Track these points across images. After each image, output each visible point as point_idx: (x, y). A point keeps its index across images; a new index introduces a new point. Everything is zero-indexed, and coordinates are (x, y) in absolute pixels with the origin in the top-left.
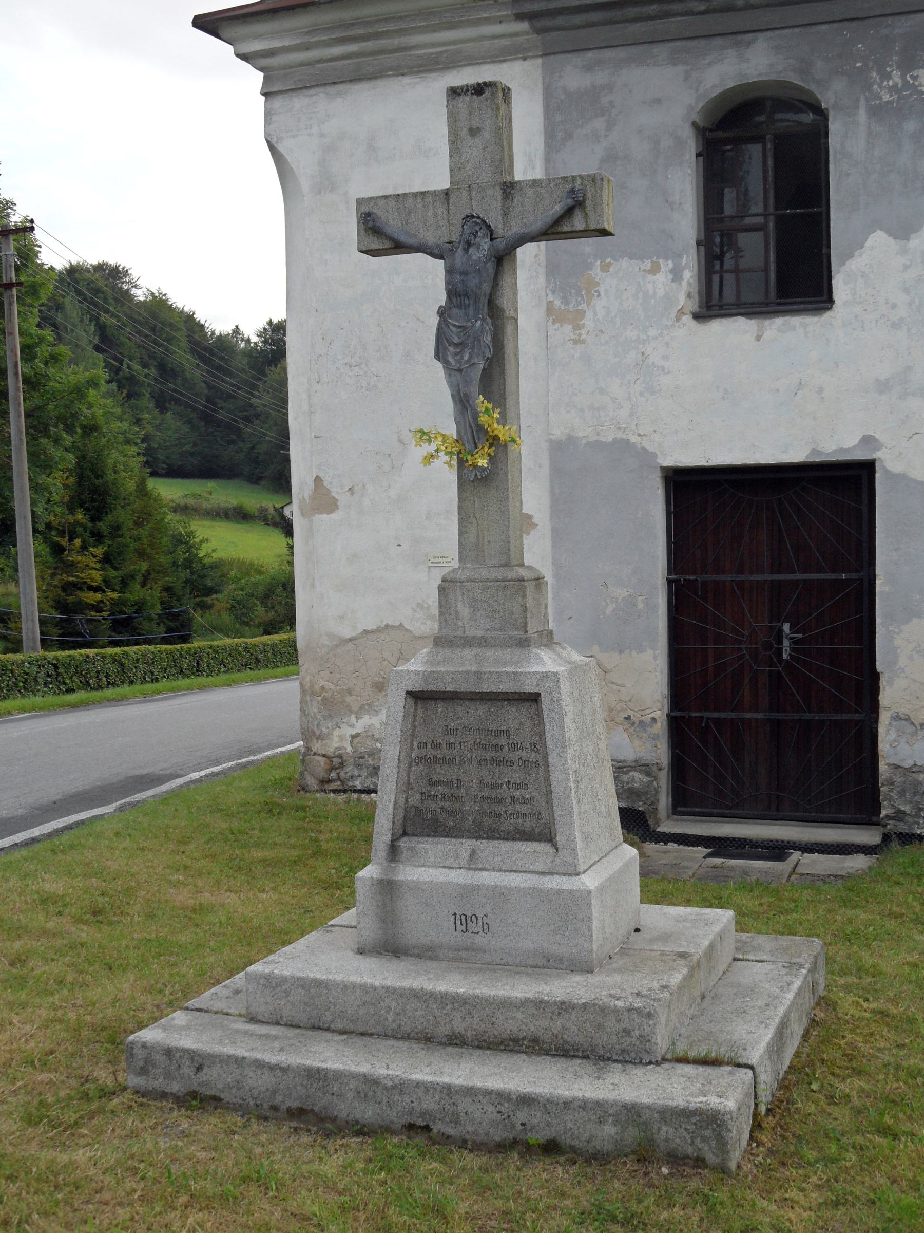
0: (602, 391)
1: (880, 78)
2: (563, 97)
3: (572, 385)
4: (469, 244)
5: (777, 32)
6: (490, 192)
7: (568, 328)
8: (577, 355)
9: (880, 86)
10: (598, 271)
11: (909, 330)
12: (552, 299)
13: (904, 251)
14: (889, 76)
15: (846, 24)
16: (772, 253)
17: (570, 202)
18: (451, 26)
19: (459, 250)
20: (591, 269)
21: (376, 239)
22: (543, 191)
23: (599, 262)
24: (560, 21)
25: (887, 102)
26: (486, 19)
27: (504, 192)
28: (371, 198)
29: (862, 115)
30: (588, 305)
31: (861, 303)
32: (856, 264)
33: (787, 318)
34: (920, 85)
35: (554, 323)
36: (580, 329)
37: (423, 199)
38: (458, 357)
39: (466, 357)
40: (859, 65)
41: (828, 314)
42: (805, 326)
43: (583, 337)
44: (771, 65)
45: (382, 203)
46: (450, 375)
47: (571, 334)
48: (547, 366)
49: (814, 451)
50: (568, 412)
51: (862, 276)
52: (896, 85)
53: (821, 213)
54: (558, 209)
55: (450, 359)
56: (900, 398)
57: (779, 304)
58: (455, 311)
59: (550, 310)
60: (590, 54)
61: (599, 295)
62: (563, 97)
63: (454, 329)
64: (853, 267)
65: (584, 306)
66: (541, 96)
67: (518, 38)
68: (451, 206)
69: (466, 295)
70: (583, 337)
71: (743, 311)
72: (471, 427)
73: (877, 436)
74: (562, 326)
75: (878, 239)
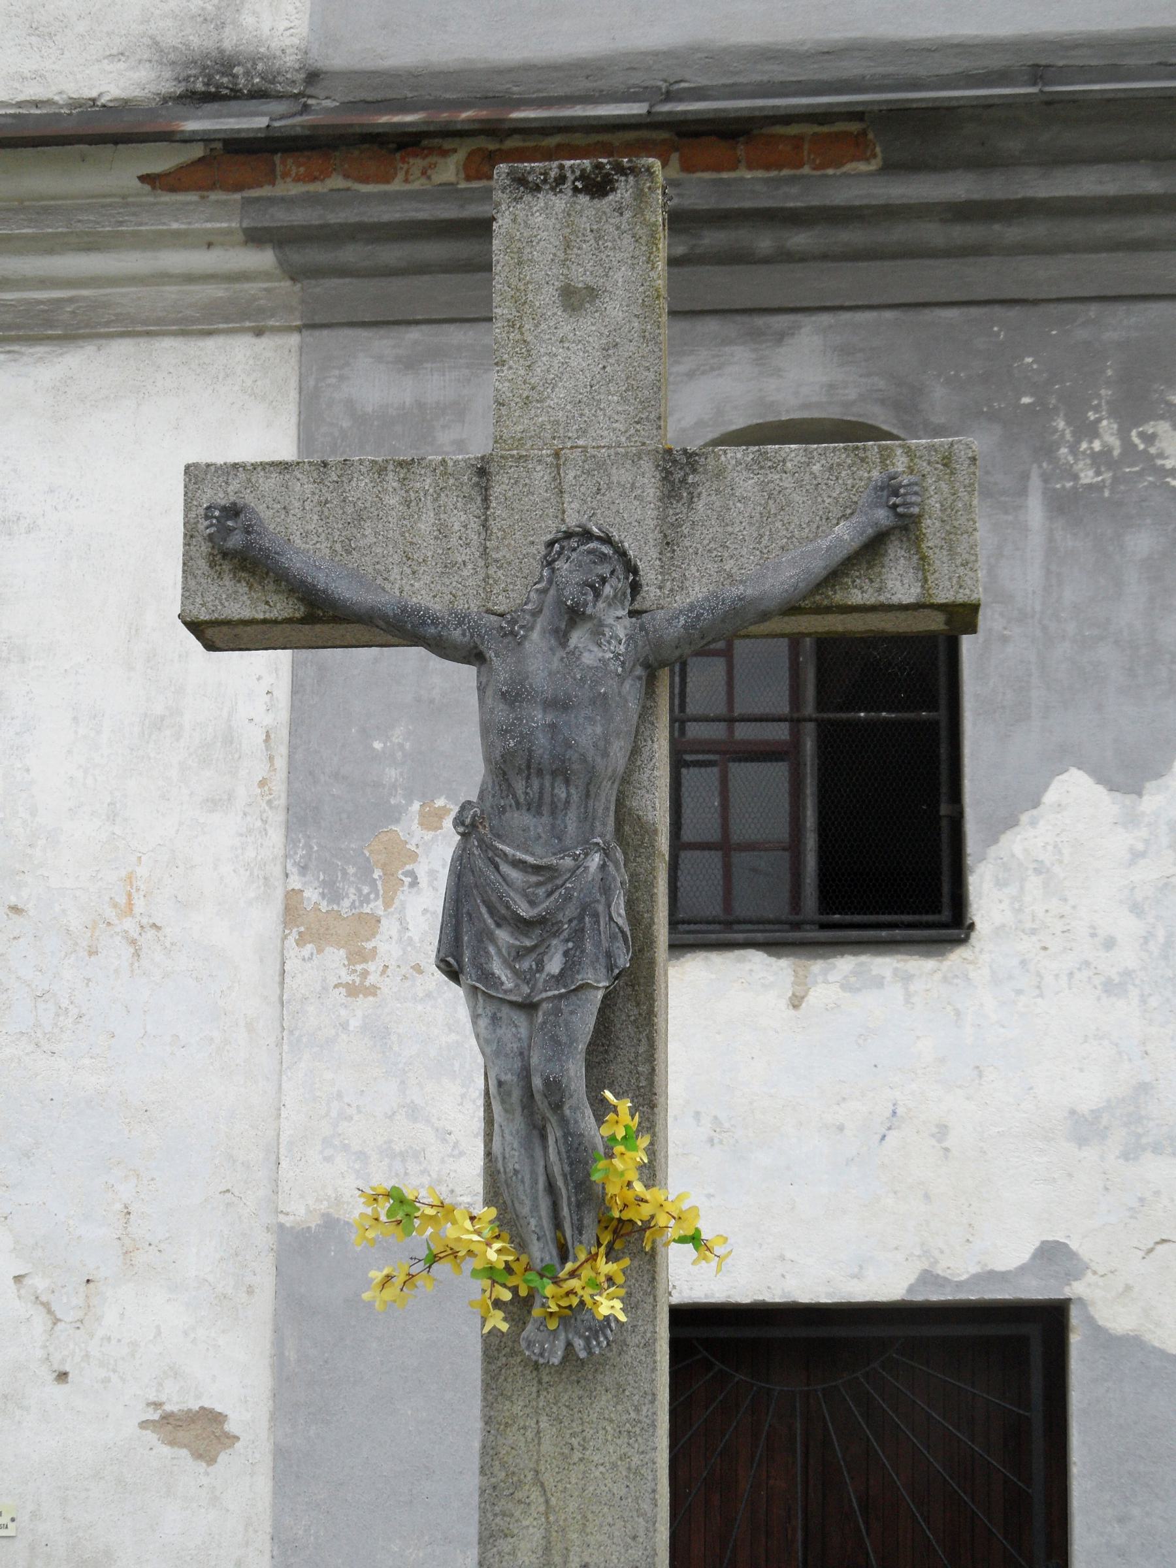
0: (414, 1113)
1: (1074, 433)
2: (346, 424)
3: (340, 1095)
4: (574, 615)
5: (846, 316)
6: (621, 475)
7: (335, 957)
8: (354, 1024)
9: (1074, 450)
10: (415, 826)
11: (1143, 1000)
12: (298, 886)
13: (1131, 820)
14: (1092, 431)
15: (998, 310)
16: (809, 813)
17: (882, 516)
18: (91, 244)
19: (535, 635)
20: (397, 821)
21: (243, 588)
22: (788, 482)
23: (416, 806)
24: (350, 254)
25: (1090, 487)
26: (177, 234)
27: (667, 477)
28: (235, 466)
29: (1035, 511)
30: (387, 905)
31: (1033, 932)
32: (1026, 842)
33: (864, 958)
34: (1161, 455)
35: (301, 941)
36: (365, 960)
37: (403, 481)
38: (526, 964)
39: (554, 965)
40: (1026, 400)
41: (957, 957)
42: (907, 978)
43: (372, 979)
44: (831, 387)
45: (269, 483)
46: (495, 1019)
47: (343, 972)
48: (279, 1044)
49: (928, 1278)
50: (328, 1159)
51: (1037, 871)
52: (1107, 451)
53: (934, 725)
54: (845, 535)
55: (497, 968)
56: (1126, 1156)
57: (824, 926)
58: (521, 819)
59: (292, 909)
60: (414, 334)
61: (414, 883)
62: (346, 424)
63: (514, 874)
64: (1017, 849)
65: (376, 906)
66: (294, 420)
67: (247, 286)
68: (497, 508)
69: (562, 773)
70: (372, 979)
71: (760, 937)
72: (551, 1188)
73: (1074, 1245)
74: (320, 951)
75: (1074, 793)
